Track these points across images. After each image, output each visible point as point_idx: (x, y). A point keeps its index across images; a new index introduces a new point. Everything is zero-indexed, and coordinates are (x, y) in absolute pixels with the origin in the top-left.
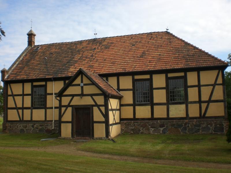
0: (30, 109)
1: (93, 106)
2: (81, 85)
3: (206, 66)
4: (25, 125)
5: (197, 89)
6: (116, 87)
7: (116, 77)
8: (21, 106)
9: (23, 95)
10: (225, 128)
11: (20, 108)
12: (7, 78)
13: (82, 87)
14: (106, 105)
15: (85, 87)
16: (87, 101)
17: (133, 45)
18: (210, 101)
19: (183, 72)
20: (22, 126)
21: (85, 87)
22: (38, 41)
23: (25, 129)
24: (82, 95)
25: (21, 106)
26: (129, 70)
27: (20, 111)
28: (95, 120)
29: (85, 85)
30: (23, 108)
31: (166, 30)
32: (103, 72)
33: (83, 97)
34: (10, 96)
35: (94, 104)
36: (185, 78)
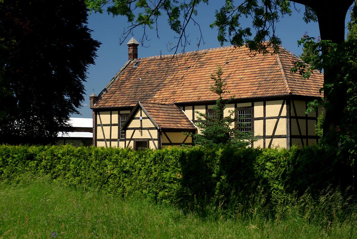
0: (117, 141)
1: (149, 140)
2: (140, 118)
3: (271, 95)
5: (262, 121)
6: (190, 119)
8: (305, 134)
9: (111, 125)
11: (108, 140)
13: (141, 120)
16: (146, 135)
17: (189, 68)
18: (273, 137)
19: (234, 103)
21: (143, 120)
24: (141, 129)
25: (305, 134)
26: (203, 99)
27: (305, 140)
29: (144, 118)
30: (111, 140)
32: (180, 101)
35: (150, 138)
36: (251, 110)
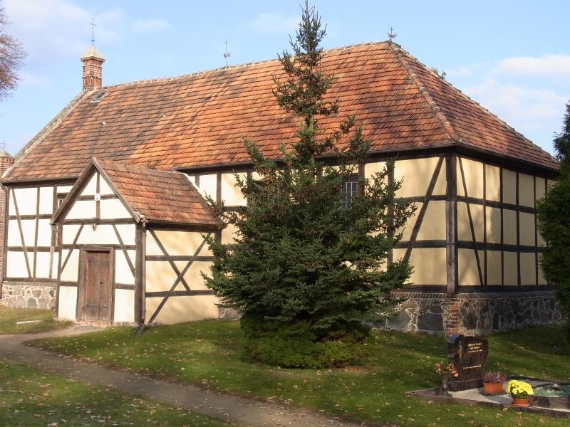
1: (116, 247)
4: (38, 288)
7: (216, 175)
10: (445, 319)
11: (30, 249)
12: (8, 176)
14: (140, 246)
15: (102, 202)
20: (31, 292)
22: (112, 77)
23: (37, 299)
27: (31, 255)
28: (118, 281)
29: (104, 197)
31: (388, 39)
33: (99, 226)
34: (13, 218)
